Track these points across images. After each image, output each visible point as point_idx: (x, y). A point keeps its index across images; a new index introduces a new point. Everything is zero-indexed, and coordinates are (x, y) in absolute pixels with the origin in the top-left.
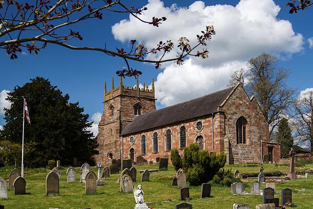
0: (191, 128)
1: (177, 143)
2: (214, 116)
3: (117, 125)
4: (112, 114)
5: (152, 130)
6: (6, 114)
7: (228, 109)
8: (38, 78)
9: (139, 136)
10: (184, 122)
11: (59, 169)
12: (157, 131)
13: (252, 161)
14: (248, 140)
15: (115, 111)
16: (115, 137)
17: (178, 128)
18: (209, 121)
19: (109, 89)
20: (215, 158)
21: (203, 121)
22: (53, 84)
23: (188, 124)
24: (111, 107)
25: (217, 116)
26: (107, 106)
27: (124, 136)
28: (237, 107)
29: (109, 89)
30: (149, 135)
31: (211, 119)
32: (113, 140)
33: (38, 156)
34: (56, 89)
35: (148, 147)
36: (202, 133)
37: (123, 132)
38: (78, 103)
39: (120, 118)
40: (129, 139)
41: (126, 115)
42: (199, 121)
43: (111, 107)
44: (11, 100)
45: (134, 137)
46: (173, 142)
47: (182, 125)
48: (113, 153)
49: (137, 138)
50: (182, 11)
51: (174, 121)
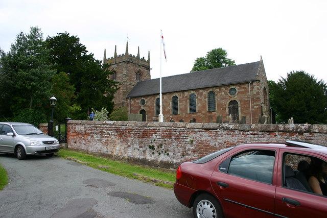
1: (204, 107)
12: (177, 95)
17: (205, 93)
21: (237, 88)
23: (218, 90)
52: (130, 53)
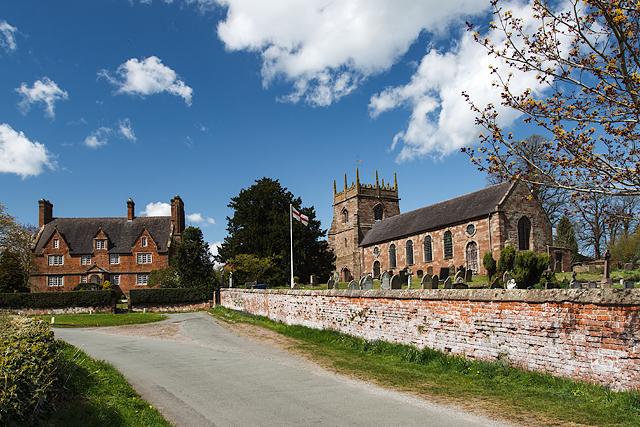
0: (459, 233)
1: (440, 252)
2: (490, 217)
3: (354, 233)
4: (346, 220)
5: (405, 237)
6: (230, 225)
7: (508, 208)
8: (265, 179)
9: (387, 246)
10: (449, 225)
11: (295, 288)
12: (411, 238)
13: (300, 299)
14: (531, 246)
15: (351, 215)
16: (352, 247)
17: (441, 233)
18: (484, 223)
19: (341, 188)
20: (542, 260)
21: (475, 223)
22: (283, 186)
23: (455, 228)
24: (345, 211)
25: (496, 217)
26: (338, 210)
27: (364, 246)
28: (518, 205)
29: (341, 188)
30: (401, 244)
31: (487, 220)
32: (351, 250)
33: (275, 272)
34: (286, 192)
35: (399, 258)
36: (475, 239)
37: (363, 243)
38: (313, 208)
39: (358, 223)
40: (371, 249)
41: (365, 221)
42: (470, 223)
43: (345, 211)
44: (235, 206)
45: (380, 247)
46: (434, 250)
47: (447, 229)
48: (351, 268)
49: (384, 248)
50: (162, 65)
51: (434, 225)
52: (361, 182)
